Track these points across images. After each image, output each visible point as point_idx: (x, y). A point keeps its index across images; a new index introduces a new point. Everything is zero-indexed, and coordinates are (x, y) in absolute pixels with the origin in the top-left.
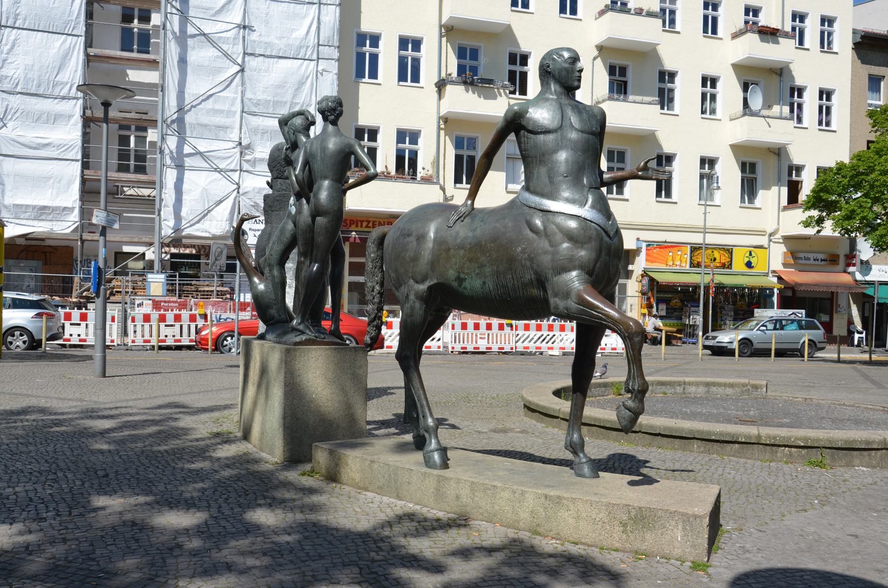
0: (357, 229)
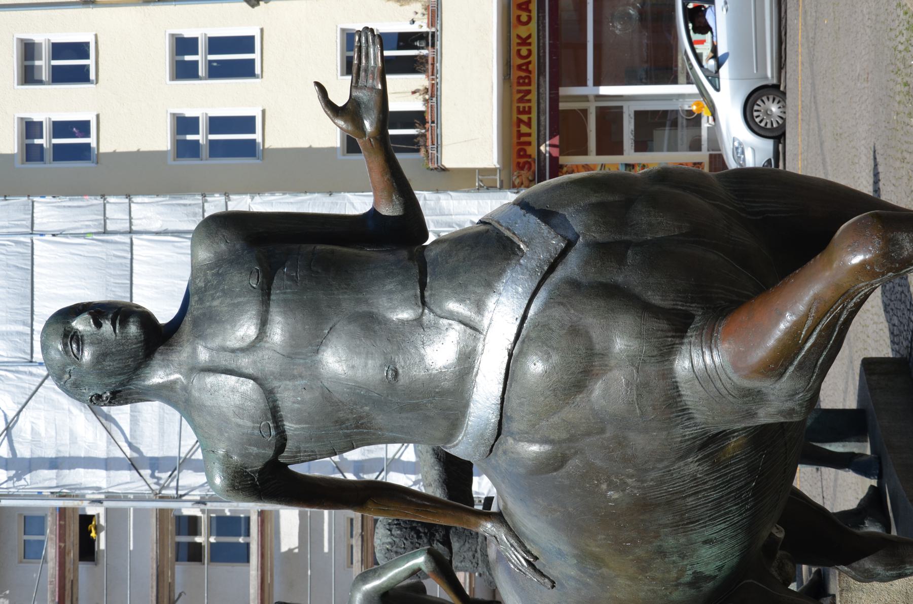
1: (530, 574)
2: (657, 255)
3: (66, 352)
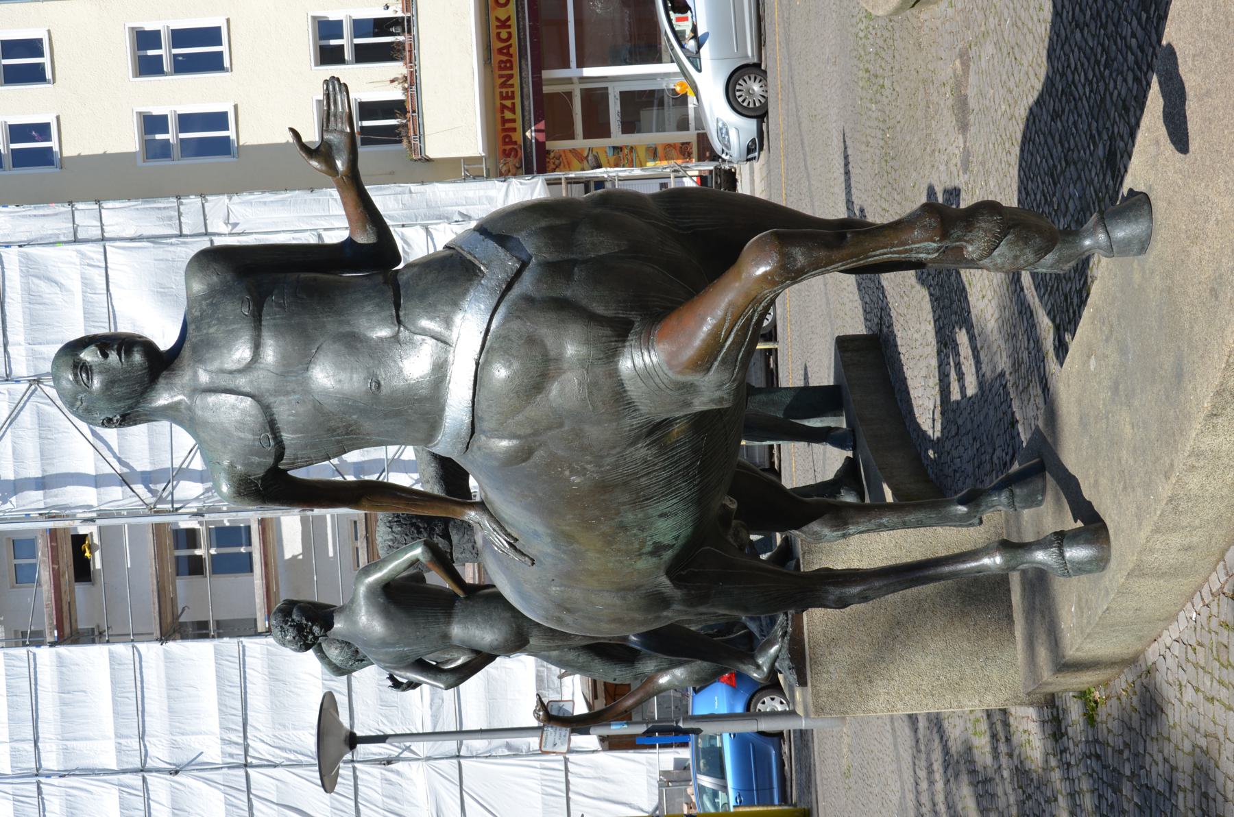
0: (520, 129)
1: (512, 554)
2: (600, 271)
3: (76, 381)
